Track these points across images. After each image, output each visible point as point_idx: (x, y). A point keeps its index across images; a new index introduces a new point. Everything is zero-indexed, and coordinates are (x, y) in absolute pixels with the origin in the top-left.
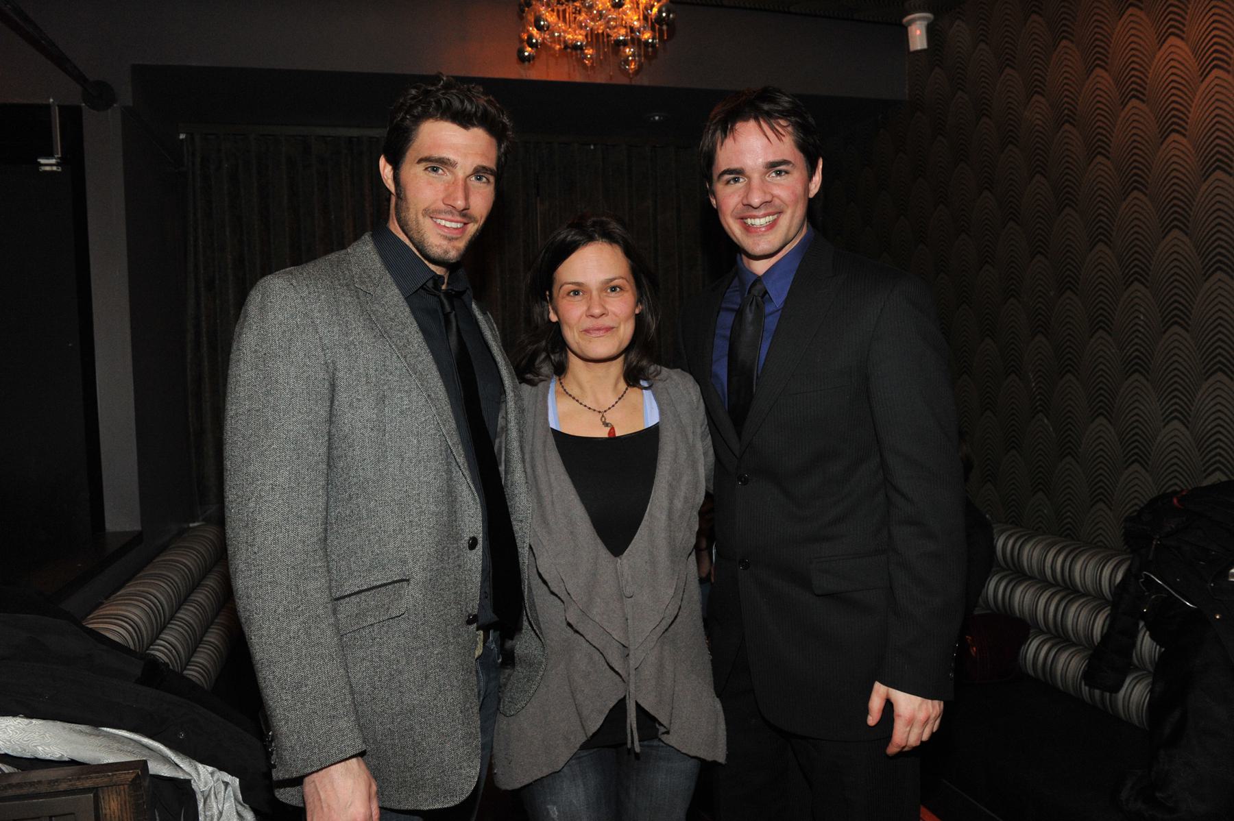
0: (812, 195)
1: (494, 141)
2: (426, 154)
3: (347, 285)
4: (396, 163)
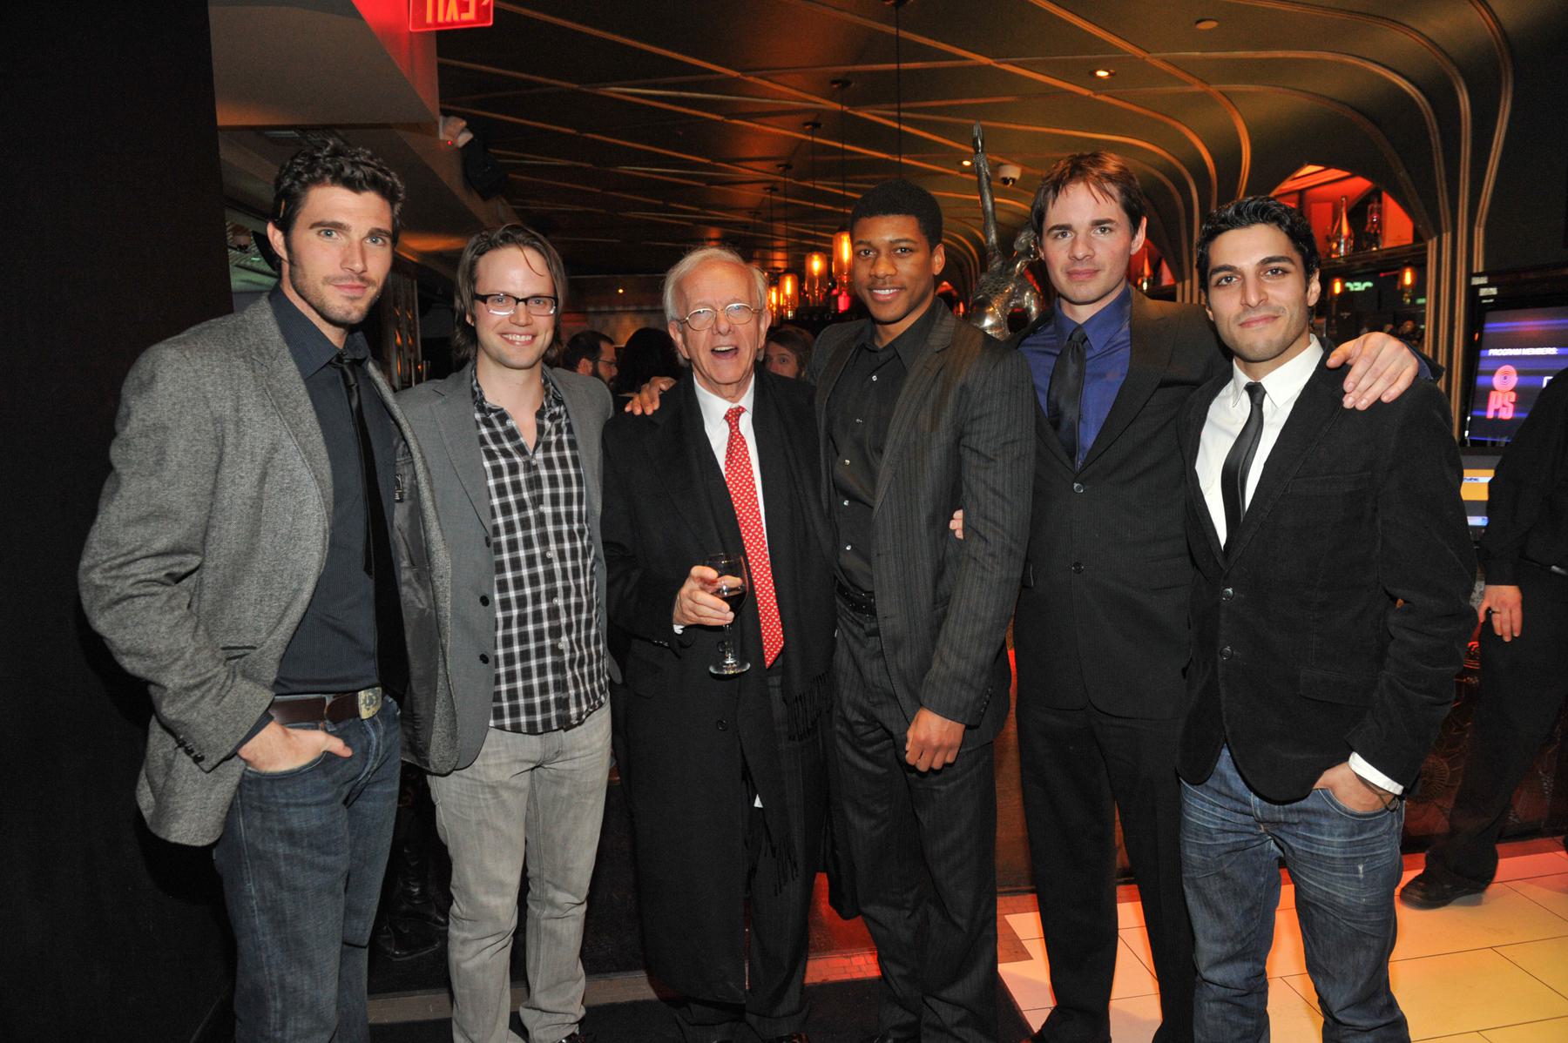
0: (1133, 252)
1: (387, 204)
2: (318, 220)
3: (244, 357)
4: (286, 227)
